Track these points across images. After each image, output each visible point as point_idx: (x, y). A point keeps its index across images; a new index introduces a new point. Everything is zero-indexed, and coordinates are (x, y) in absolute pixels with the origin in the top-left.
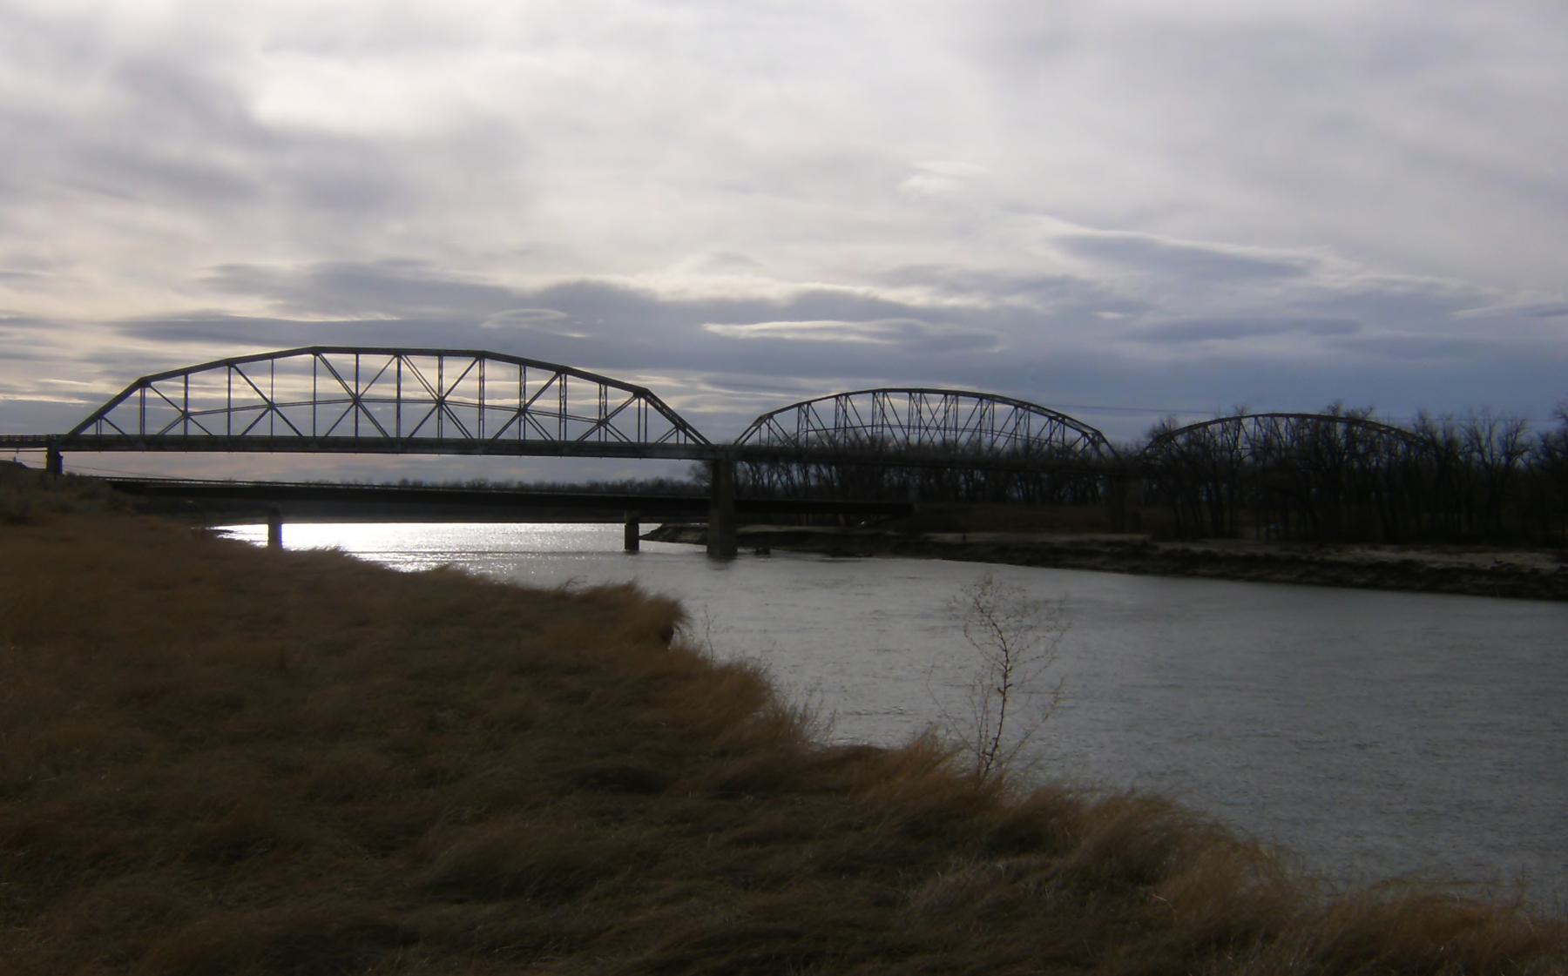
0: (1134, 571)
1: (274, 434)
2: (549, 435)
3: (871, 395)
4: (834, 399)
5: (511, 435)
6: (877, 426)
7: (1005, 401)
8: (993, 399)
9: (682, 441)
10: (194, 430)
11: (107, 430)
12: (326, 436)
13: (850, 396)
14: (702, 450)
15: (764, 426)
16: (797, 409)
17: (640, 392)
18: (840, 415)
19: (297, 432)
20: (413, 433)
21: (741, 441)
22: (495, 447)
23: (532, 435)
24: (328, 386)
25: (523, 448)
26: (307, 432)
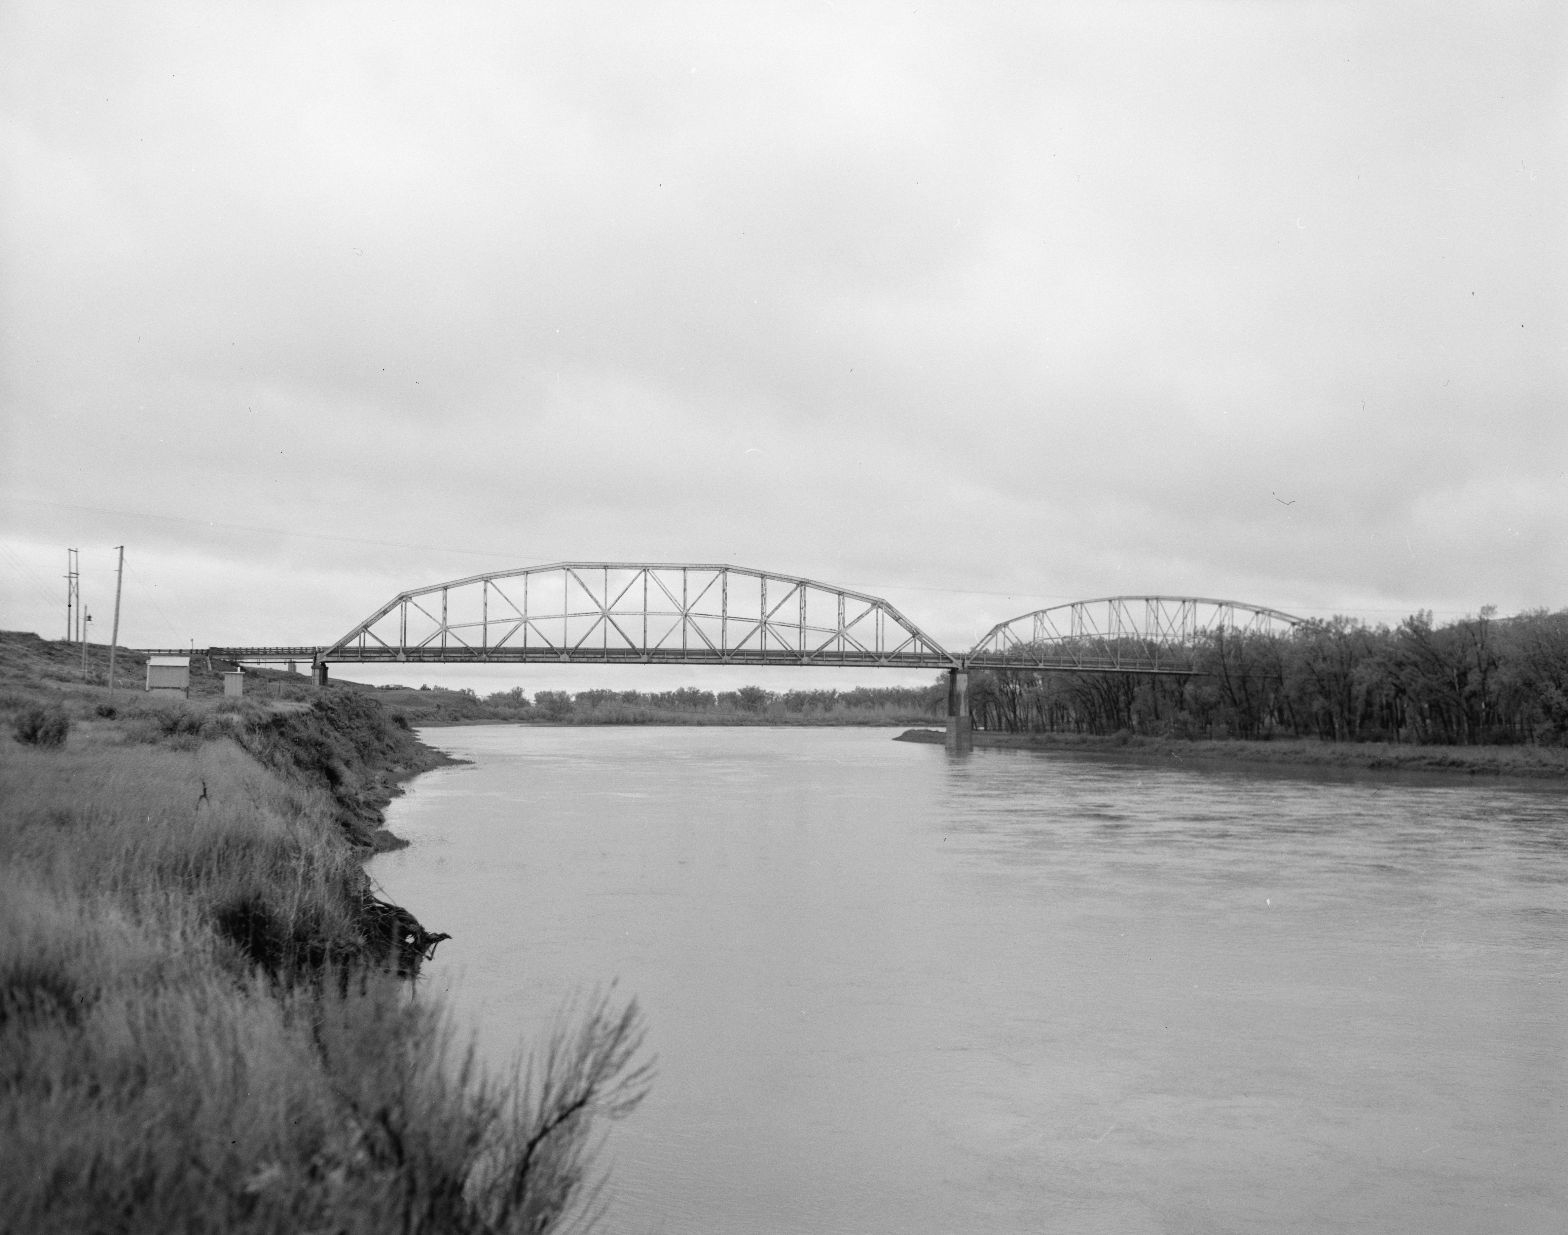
0: (931, 742)
1: (608, 647)
2: (789, 646)
3: (1107, 603)
4: (1070, 608)
5: (753, 644)
6: (1114, 634)
7: (1245, 607)
8: (1230, 604)
9: (918, 651)
10: (452, 643)
11: (371, 643)
12: (577, 647)
13: (1086, 605)
14: (938, 658)
15: (1000, 634)
16: (1032, 617)
17: (877, 604)
18: (1152, 622)
19: (549, 644)
20: (579, 644)
21: (978, 649)
22: (820, 658)
23: (773, 645)
24: (581, 601)
25: (841, 659)
26: (558, 644)
